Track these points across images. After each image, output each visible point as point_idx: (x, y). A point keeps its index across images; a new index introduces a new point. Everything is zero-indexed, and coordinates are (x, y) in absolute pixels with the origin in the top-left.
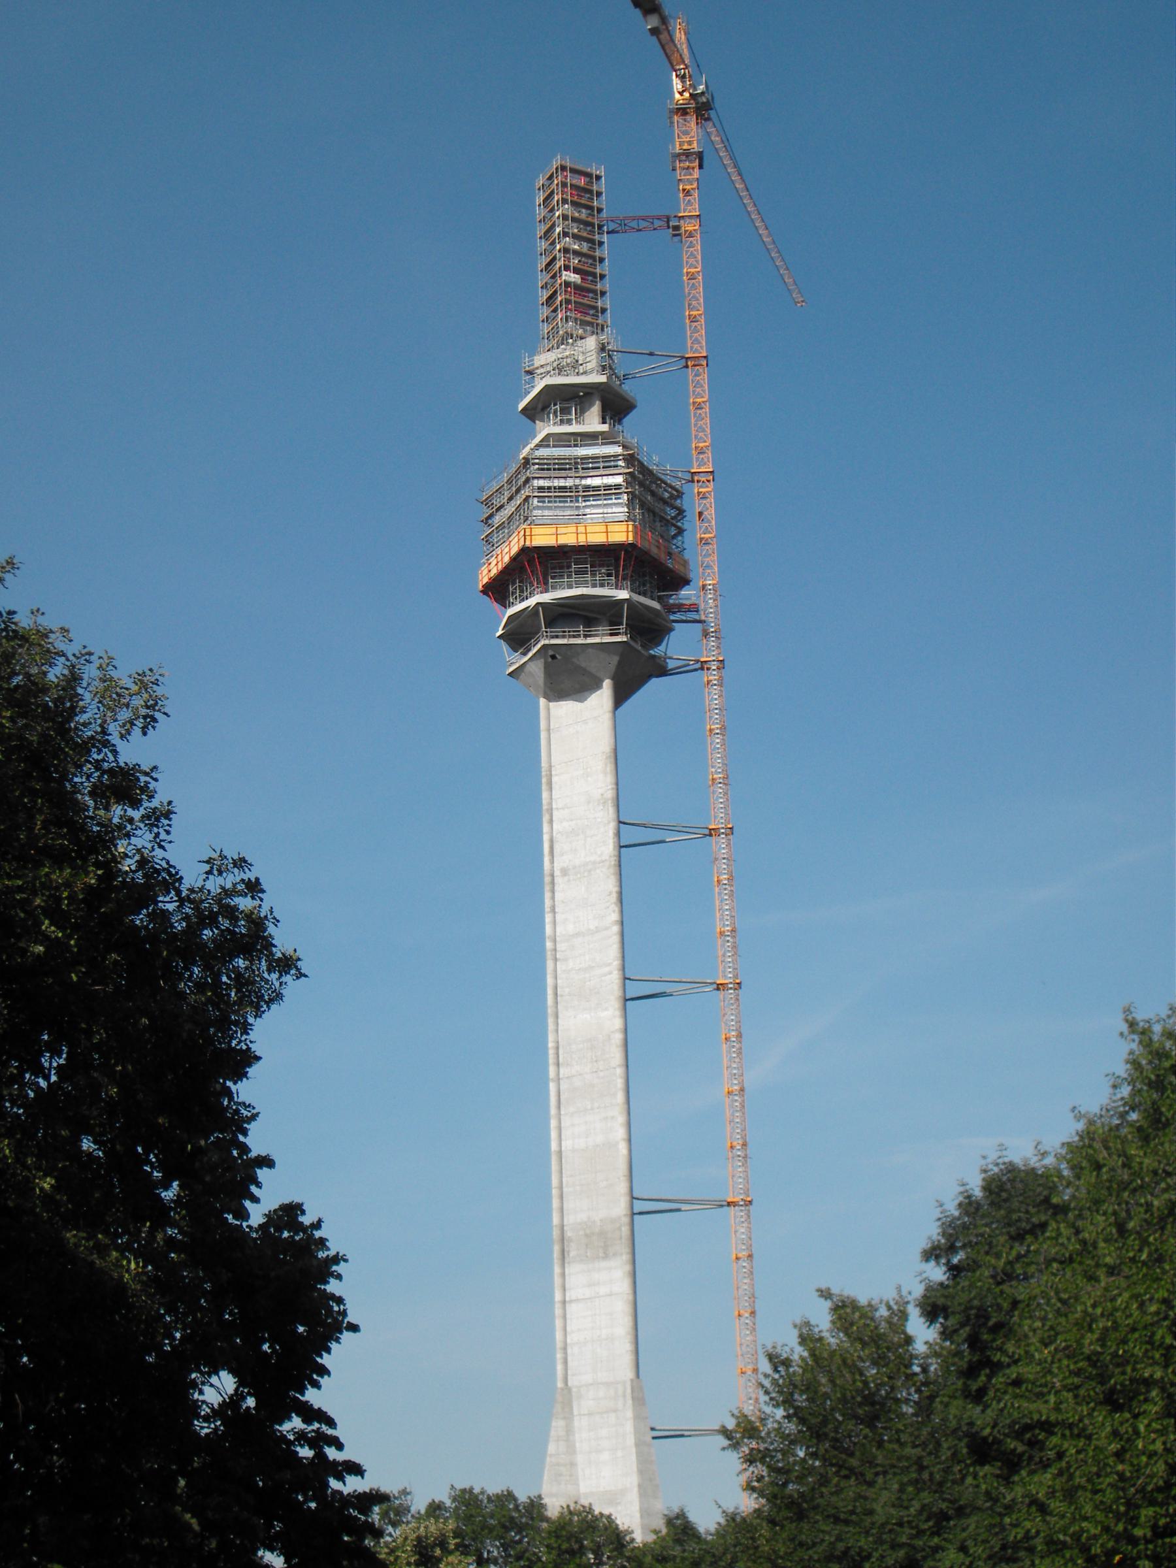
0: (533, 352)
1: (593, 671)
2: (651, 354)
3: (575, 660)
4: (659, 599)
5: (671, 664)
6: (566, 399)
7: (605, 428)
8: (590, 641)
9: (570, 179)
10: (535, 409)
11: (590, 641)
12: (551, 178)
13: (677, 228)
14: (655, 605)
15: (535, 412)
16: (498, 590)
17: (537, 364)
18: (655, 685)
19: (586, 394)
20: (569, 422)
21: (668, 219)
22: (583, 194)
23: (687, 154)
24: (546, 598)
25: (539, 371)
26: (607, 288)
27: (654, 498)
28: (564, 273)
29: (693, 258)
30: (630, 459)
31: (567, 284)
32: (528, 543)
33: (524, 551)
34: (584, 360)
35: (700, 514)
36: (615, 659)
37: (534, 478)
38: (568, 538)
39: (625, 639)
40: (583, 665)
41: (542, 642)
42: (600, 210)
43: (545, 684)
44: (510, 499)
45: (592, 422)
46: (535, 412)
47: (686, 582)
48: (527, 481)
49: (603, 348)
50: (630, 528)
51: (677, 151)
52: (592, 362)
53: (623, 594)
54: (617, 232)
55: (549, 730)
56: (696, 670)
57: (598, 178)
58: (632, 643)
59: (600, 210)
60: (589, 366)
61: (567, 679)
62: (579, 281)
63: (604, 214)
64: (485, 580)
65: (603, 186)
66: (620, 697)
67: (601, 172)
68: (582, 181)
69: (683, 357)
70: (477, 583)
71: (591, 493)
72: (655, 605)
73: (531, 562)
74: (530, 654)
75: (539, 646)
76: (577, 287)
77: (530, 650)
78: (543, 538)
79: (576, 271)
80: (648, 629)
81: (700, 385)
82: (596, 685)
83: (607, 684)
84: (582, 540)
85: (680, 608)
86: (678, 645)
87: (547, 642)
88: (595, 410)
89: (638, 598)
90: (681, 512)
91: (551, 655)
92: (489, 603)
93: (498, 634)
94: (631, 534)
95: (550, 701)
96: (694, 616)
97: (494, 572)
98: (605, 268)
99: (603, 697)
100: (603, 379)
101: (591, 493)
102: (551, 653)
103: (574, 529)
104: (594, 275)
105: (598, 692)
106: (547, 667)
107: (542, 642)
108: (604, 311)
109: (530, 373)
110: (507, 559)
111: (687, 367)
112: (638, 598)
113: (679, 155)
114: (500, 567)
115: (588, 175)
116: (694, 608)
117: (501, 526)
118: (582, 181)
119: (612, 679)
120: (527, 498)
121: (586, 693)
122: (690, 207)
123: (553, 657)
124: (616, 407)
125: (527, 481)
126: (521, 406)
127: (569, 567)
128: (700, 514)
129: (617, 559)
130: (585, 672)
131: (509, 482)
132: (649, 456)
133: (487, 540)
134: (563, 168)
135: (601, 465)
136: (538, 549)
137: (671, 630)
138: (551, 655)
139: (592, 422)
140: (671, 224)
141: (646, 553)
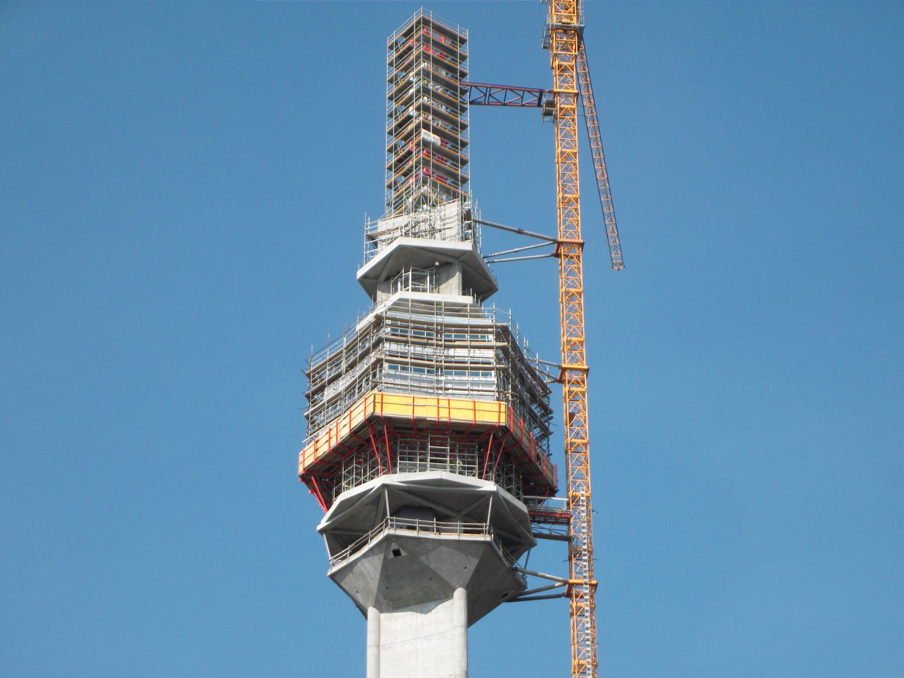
0: (379, 214)
1: (444, 575)
2: (520, 232)
3: (423, 558)
4: (526, 502)
5: (532, 583)
6: (427, 265)
7: (468, 300)
8: (445, 536)
9: (432, 35)
10: (377, 278)
11: (445, 536)
12: (408, 34)
13: (551, 104)
14: (524, 508)
15: (375, 282)
16: (325, 476)
17: (380, 230)
18: (505, 609)
19: (444, 265)
20: (424, 291)
21: (541, 92)
22: (447, 52)
23: (566, 29)
24: (396, 479)
25: (383, 237)
26: (468, 157)
27: (524, 384)
28: (423, 131)
29: (567, 140)
30: (503, 333)
31: (426, 144)
32: (378, 412)
33: (372, 421)
34: (444, 227)
35: (572, 416)
36: (473, 563)
37: (388, 340)
38: (428, 409)
39: (488, 538)
40: (433, 566)
41: (387, 532)
42: (463, 75)
43: (379, 587)
44: (352, 366)
45: (451, 292)
46: (375, 282)
47: (552, 492)
48: (380, 341)
49: (467, 216)
50: (503, 409)
51: (555, 22)
52: (454, 227)
53: (489, 486)
54: (479, 103)
55: (378, 646)
56: (558, 596)
57: (463, 41)
58: (494, 545)
59: (463, 75)
60: (448, 233)
61: (409, 585)
62: (439, 143)
63: (467, 79)
64: (309, 461)
65: (466, 50)
66: (474, 613)
67: (466, 35)
68: (447, 42)
69: (555, 241)
70: (297, 468)
71: (459, 368)
72: (524, 508)
73: (379, 435)
74: (366, 549)
75: (381, 537)
76: (436, 150)
77: (366, 543)
78: (397, 405)
79: (436, 131)
80: (513, 538)
81: (571, 278)
82: (446, 594)
83: (460, 594)
84: (444, 416)
85: (550, 517)
86: (541, 561)
87: (392, 532)
88: (456, 281)
89: (504, 493)
90: (547, 411)
91: (394, 550)
92: (309, 498)
93: (319, 527)
94: (503, 416)
95: (381, 611)
96: (560, 529)
97: (324, 449)
98: (466, 136)
99: (454, 608)
100: (467, 246)
101: (459, 368)
102: (394, 546)
103: (435, 402)
104: (455, 140)
105: (447, 604)
106: (386, 567)
107: (387, 532)
108: (464, 180)
109: (371, 238)
110: (345, 432)
111: (557, 255)
112: (504, 493)
113: (555, 28)
114: (334, 443)
115: (453, 37)
116: (565, 520)
117: (333, 402)
118: (447, 42)
119: (466, 588)
120: (379, 362)
121: (433, 603)
122: (564, 86)
123: (397, 553)
124: (479, 284)
125: (376, 345)
126: (360, 273)
127: (423, 447)
128: (572, 416)
129: (483, 446)
130: (434, 576)
131: (351, 348)
132: (521, 340)
133: (311, 419)
134: (426, 22)
135: (443, 364)
136: (389, 421)
137: (533, 545)
138: (394, 550)
139: (451, 292)
140: (544, 100)
141: (517, 443)
